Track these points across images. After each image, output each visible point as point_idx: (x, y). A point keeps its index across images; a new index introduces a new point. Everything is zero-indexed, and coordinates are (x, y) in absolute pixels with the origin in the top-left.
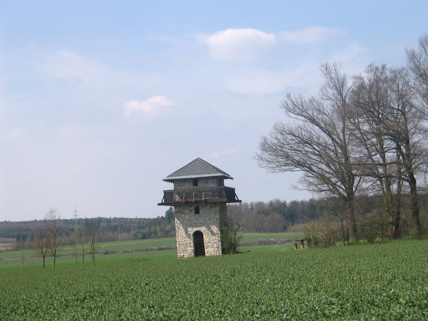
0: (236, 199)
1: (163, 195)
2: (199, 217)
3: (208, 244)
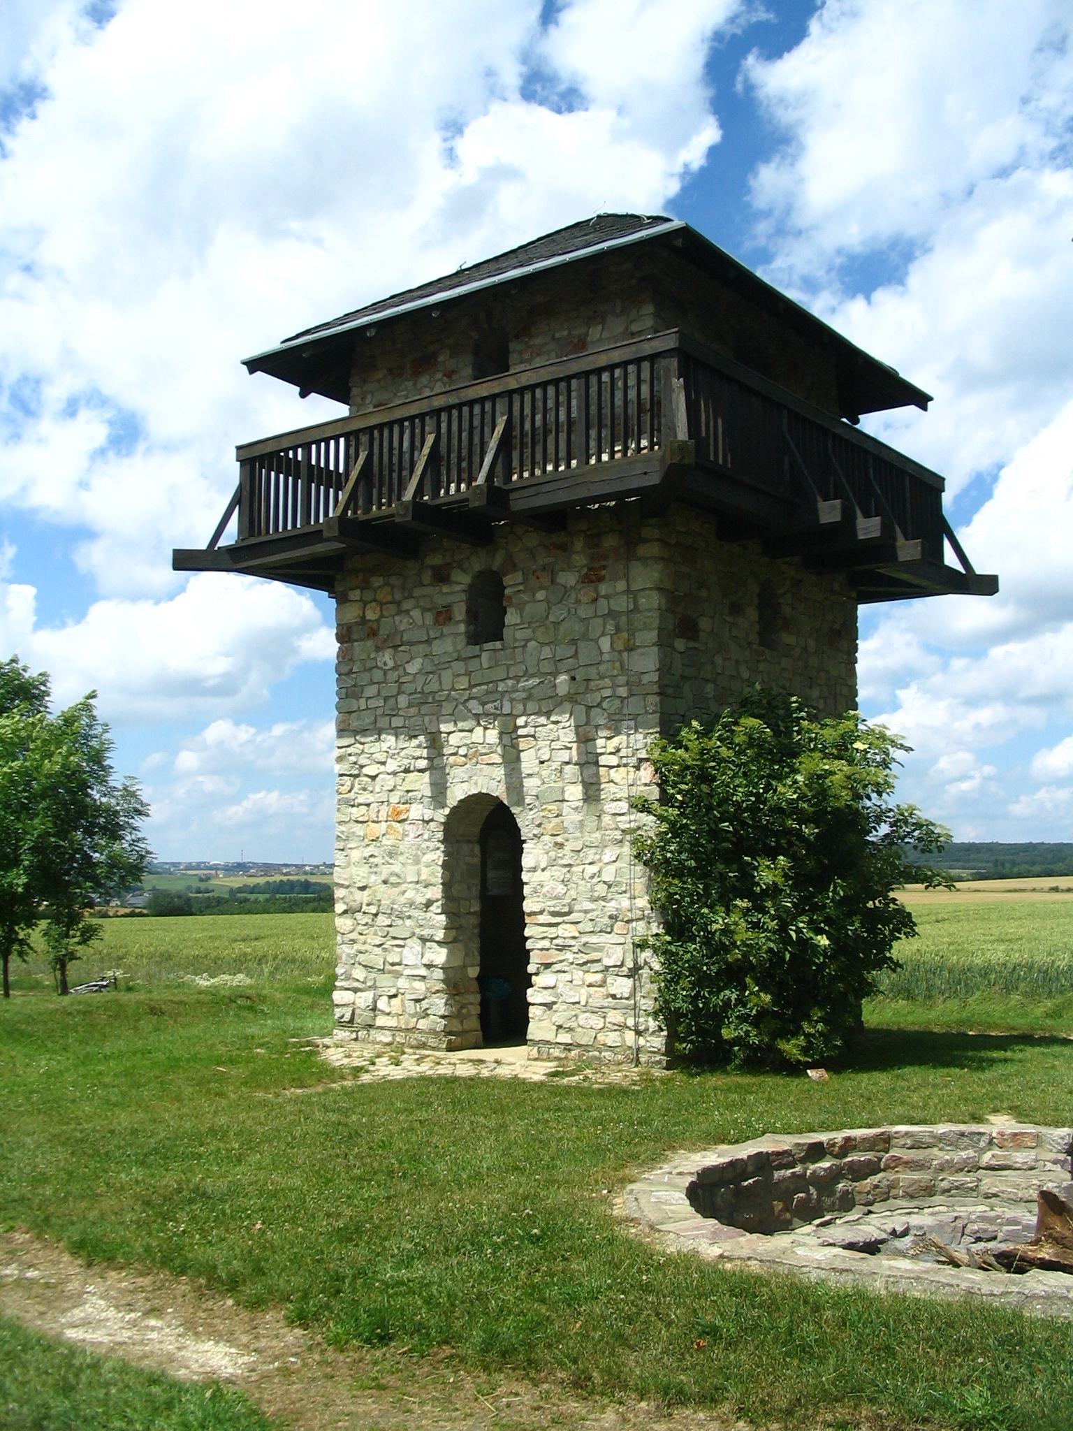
0: (950, 559)
1: (232, 473)
2: (499, 673)
3: (552, 932)
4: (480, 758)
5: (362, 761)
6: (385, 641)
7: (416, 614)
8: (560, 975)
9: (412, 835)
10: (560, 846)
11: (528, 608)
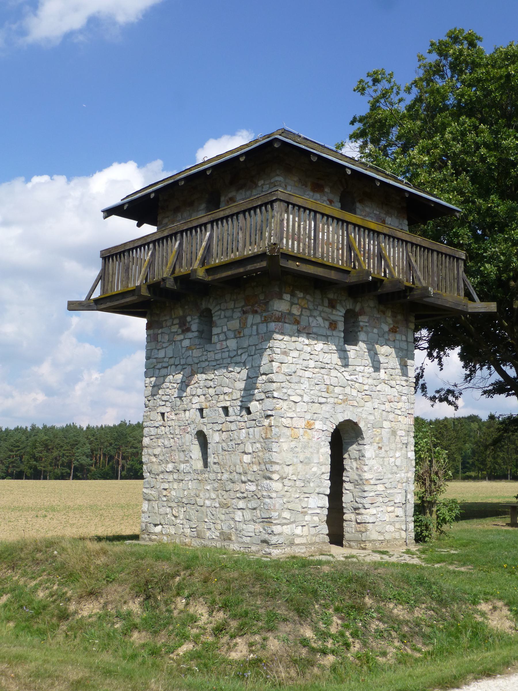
4: (349, 402)
5: (290, 392)
6: (304, 329)
7: (320, 319)
8: (377, 508)
9: (316, 437)
10: (380, 448)
11: (370, 334)
